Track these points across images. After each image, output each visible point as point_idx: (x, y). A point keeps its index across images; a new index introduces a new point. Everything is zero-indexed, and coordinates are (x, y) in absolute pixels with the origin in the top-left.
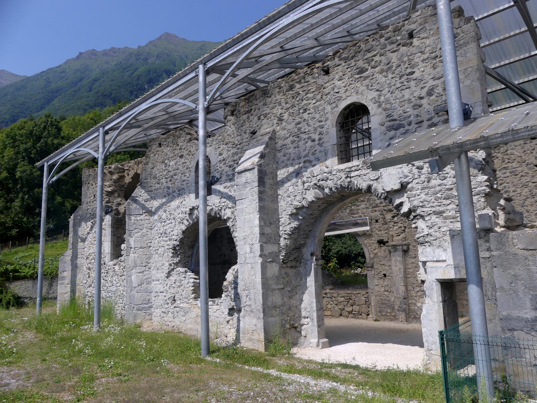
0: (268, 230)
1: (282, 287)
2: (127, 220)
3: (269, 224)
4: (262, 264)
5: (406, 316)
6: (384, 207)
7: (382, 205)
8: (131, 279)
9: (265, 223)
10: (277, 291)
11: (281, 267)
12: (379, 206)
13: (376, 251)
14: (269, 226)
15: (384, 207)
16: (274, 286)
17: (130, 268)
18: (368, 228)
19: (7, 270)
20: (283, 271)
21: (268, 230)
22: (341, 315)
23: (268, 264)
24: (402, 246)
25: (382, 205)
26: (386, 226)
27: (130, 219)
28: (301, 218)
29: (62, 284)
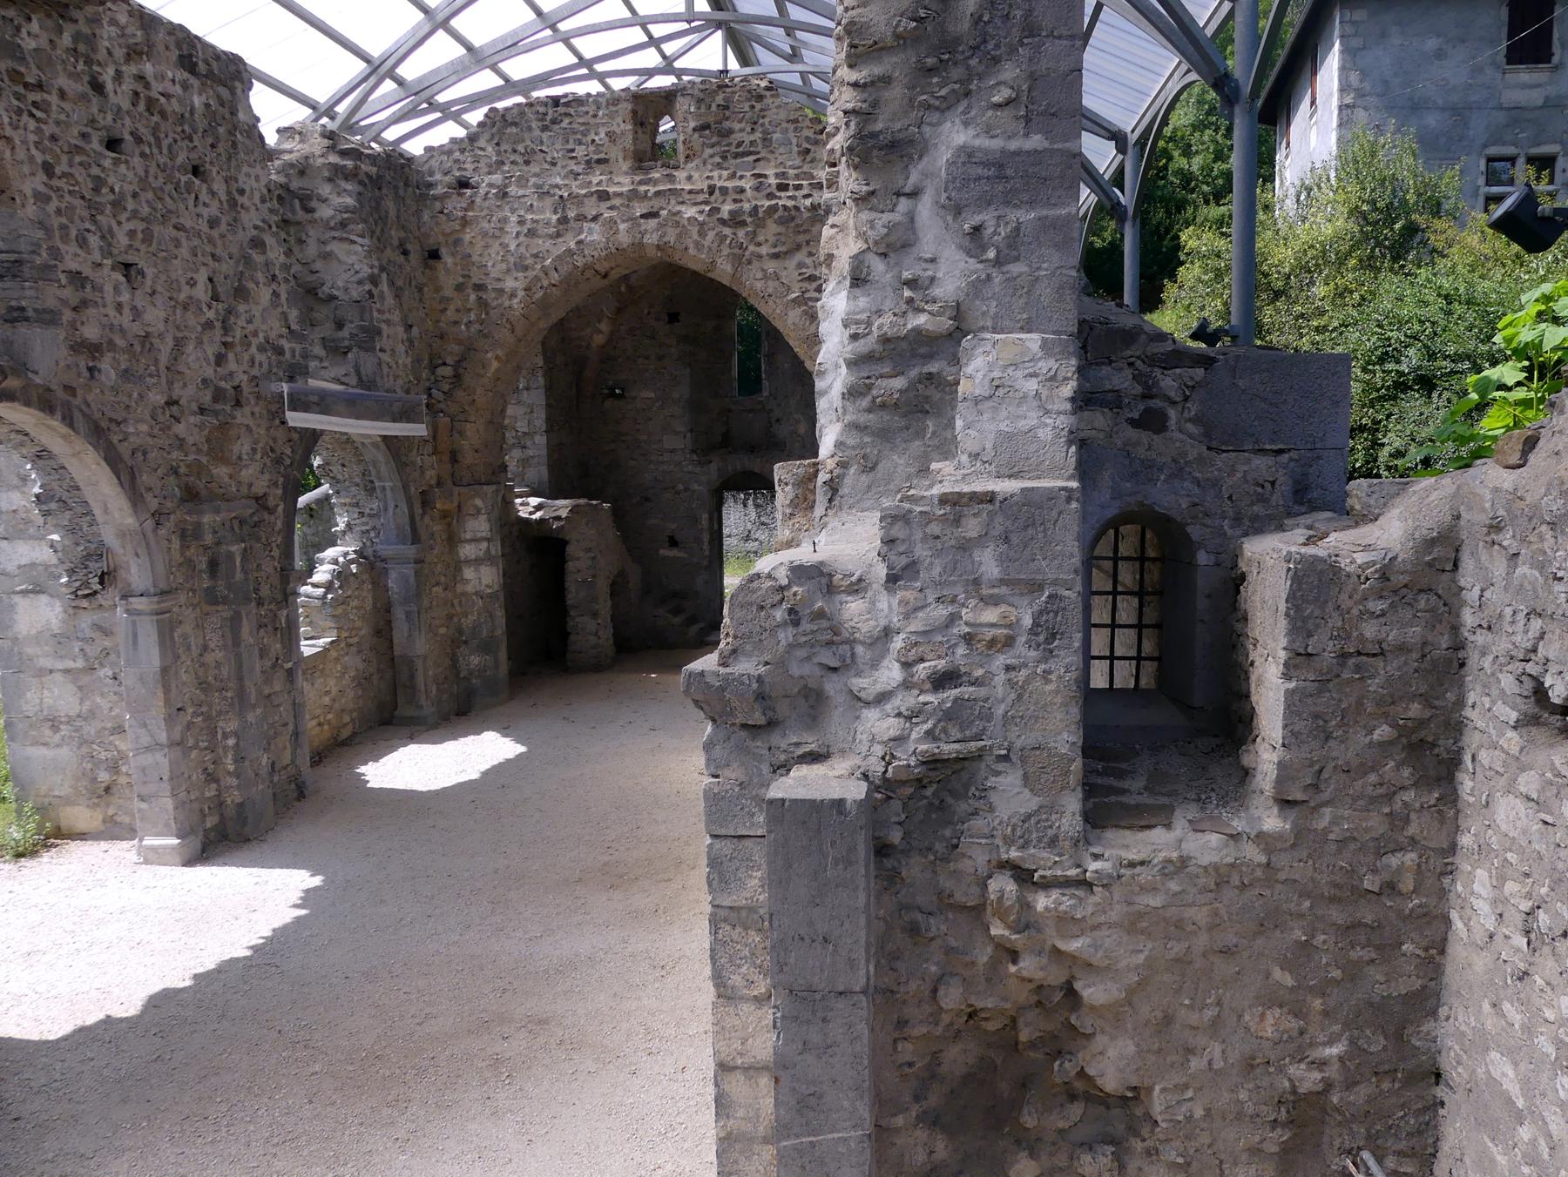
1: (80, 664)
3: (15, 481)
10: (58, 677)
20: (86, 621)
23: (17, 599)
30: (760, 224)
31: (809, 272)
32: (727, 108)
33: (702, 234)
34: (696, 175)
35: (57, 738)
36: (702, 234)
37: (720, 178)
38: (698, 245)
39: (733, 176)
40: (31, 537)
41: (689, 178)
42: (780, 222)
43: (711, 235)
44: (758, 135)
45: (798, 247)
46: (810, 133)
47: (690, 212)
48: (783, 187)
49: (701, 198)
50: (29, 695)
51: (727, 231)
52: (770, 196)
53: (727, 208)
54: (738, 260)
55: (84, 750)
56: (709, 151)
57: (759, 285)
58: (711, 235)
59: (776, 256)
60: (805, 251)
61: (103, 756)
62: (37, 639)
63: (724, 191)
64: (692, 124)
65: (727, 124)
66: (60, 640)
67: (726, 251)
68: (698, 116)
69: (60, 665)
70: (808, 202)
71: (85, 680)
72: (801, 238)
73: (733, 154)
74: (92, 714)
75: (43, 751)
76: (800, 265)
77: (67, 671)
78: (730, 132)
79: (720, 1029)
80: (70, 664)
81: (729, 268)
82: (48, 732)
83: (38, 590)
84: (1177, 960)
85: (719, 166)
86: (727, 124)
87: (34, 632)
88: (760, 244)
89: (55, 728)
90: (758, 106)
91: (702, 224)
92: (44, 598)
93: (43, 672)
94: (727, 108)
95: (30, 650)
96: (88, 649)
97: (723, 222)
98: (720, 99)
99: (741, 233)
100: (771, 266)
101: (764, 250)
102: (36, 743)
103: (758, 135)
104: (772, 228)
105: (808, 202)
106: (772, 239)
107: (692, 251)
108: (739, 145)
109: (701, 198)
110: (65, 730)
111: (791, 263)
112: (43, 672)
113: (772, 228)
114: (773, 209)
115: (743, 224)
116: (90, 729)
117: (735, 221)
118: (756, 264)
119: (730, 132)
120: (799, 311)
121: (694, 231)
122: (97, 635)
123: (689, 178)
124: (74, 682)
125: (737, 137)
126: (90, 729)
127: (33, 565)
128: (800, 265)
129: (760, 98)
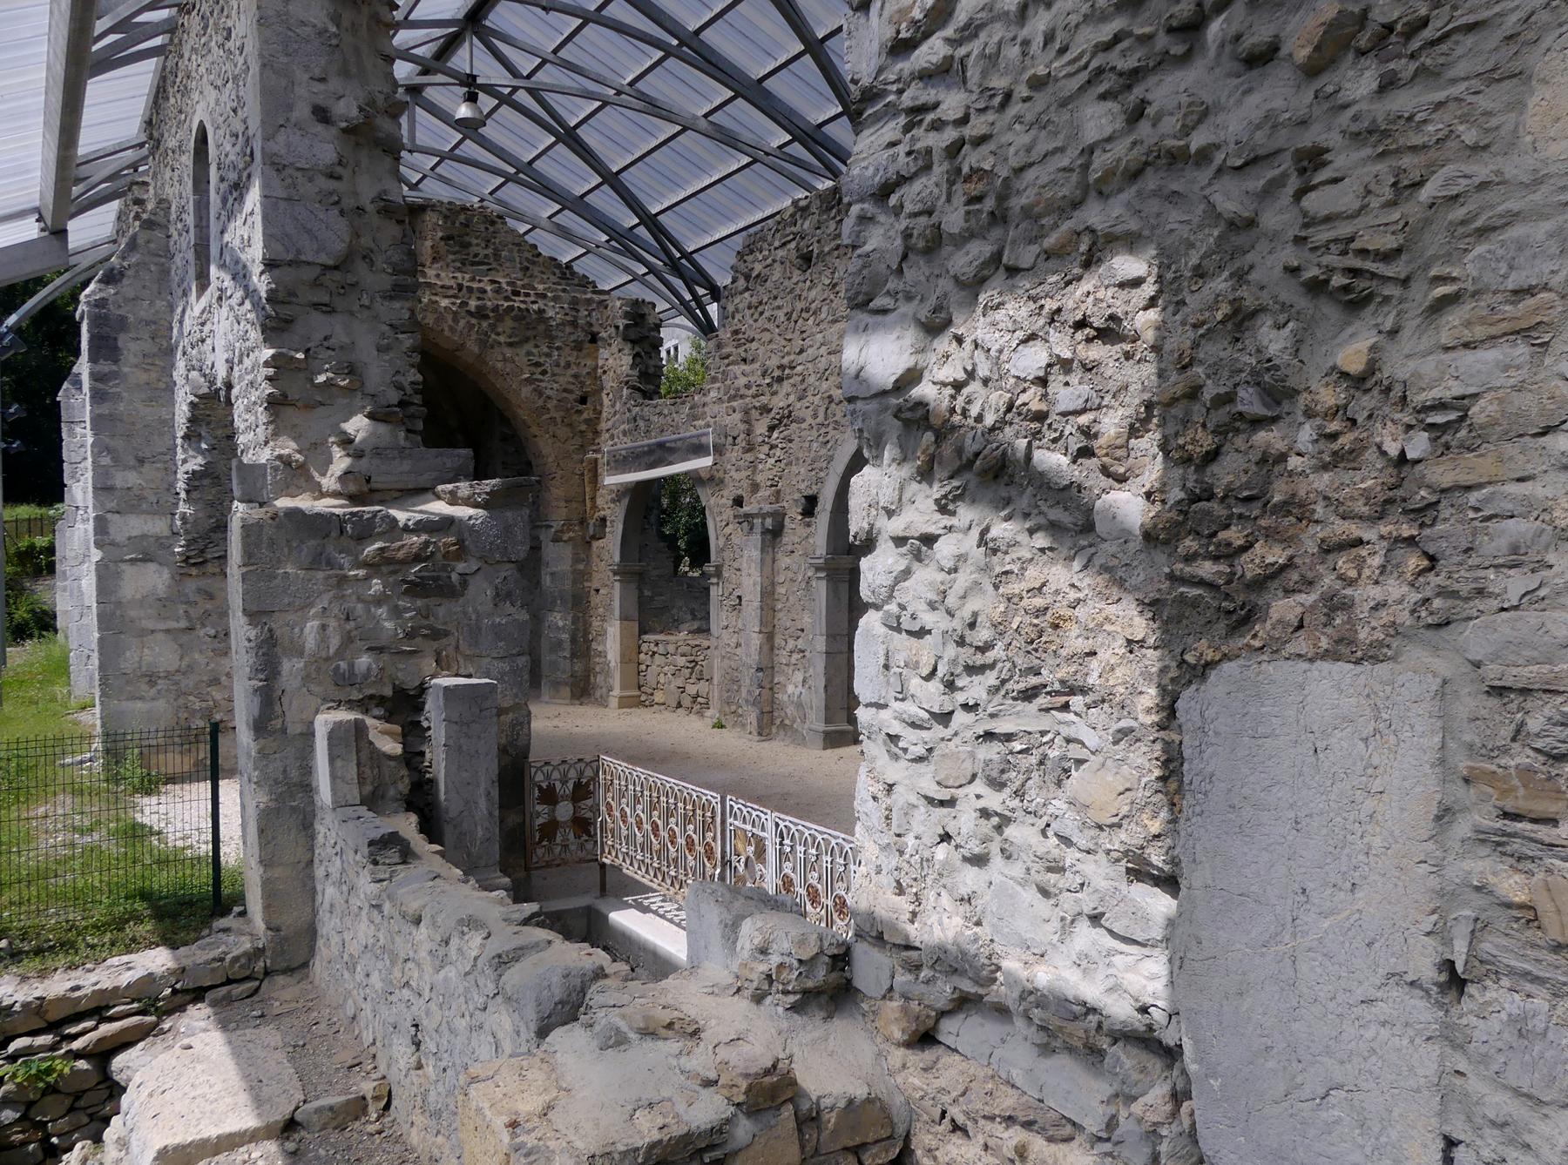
0: (127, 478)
1: (183, 624)
2: (64, 436)
3: (133, 462)
4: (101, 568)
5: (760, 720)
6: (754, 397)
7: (750, 392)
8: (79, 587)
9: (115, 459)
10: (160, 636)
11: (181, 576)
12: (742, 397)
13: (727, 530)
14: (134, 468)
15: (754, 397)
16: (149, 624)
17: (76, 557)
18: (706, 462)
19: (32, 546)
20: (191, 586)
21: (127, 478)
22: (679, 705)
23: (123, 566)
24: (764, 516)
25: (750, 392)
26: (749, 457)
27: (72, 433)
28: (204, 446)
29: (65, 590)
30: (500, 319)
31: (536, 359)
32: (467, 226)
33: (456, 320)
34: (443, 274)
35: (153, 691)
36: (456, 320)
37: (464, 278)
38: (452, 329)
39: (473, 279)
40: (143, 512)
41: (438, 276)
42: (515, 319)
43: (462, 323)
44: (489, 251)
45: (527, 340)
46: (529, 255)
47: (444, 303)
48: (517, 293)
49: (451, 292)
50: (128, 654)
51: (474, 321)
52: (507, 299)
53: (473, 304)
54: (483, 343)
55: (181, 701)
56: (451, 257)
57: (499, 365)
58: (462, 323)
59: (510, 345)
60: (532, 343)
61: (197, 706)
62: (142, 603)
63: (470, 289)
64: (440, 234)
65: (467, 239)
66: (164, 603)
67: (474, 337)
68: (443, 228)
69: (162, 626)
70: (535, 307)
71: (185, 638)
72: (530, 333)
73: (469, 262)
74: (191, 668)
75: (139, 705)
76: (529, 353)
77: (168, 631)
78: (470, 244)
79: (801, 741)
80: (172, 624)
81: (476, 350)
82: (144, 687)
83: (147, 559)
84: (1355, 303)
85: (459, 270)
86: (467, 239)
87: (138, 596)
88: (498, 334)
89: (152, 683)
90: (491, 229)
91: (455, 313)
92: (152, 567)
93: (143, 633)
94: (467, 226)
95: (133, 613)
96: (191, 611)
97: (469, 312)
98: (462, 218)
99: (485, 324)
100: (508, 352)
101: (502, 339)
102: (134, 698)
103: (489, 251)
104: (509, 323)
105: (535, 307)
106: (509, 331)
107: (447, 333)
108: (476, 255)
109: (451, 292)
110: (162, 684)
111: (522, 351)
112: (143, 633)
113: (509, 323)
114: (511, 308)
115: (486, 317)
116: (188, 683)
117: (480, 314)
118: (497, 349)
119: (470, 244)
120: (530, 388)
121: (449, 318)
122: (198, 598)
123: (438, 276)
124: (175, 640)
125: (474, 249)
126: (188, 683)
127: (144, 537)
128: (529, 353)
129: (493, 223)
